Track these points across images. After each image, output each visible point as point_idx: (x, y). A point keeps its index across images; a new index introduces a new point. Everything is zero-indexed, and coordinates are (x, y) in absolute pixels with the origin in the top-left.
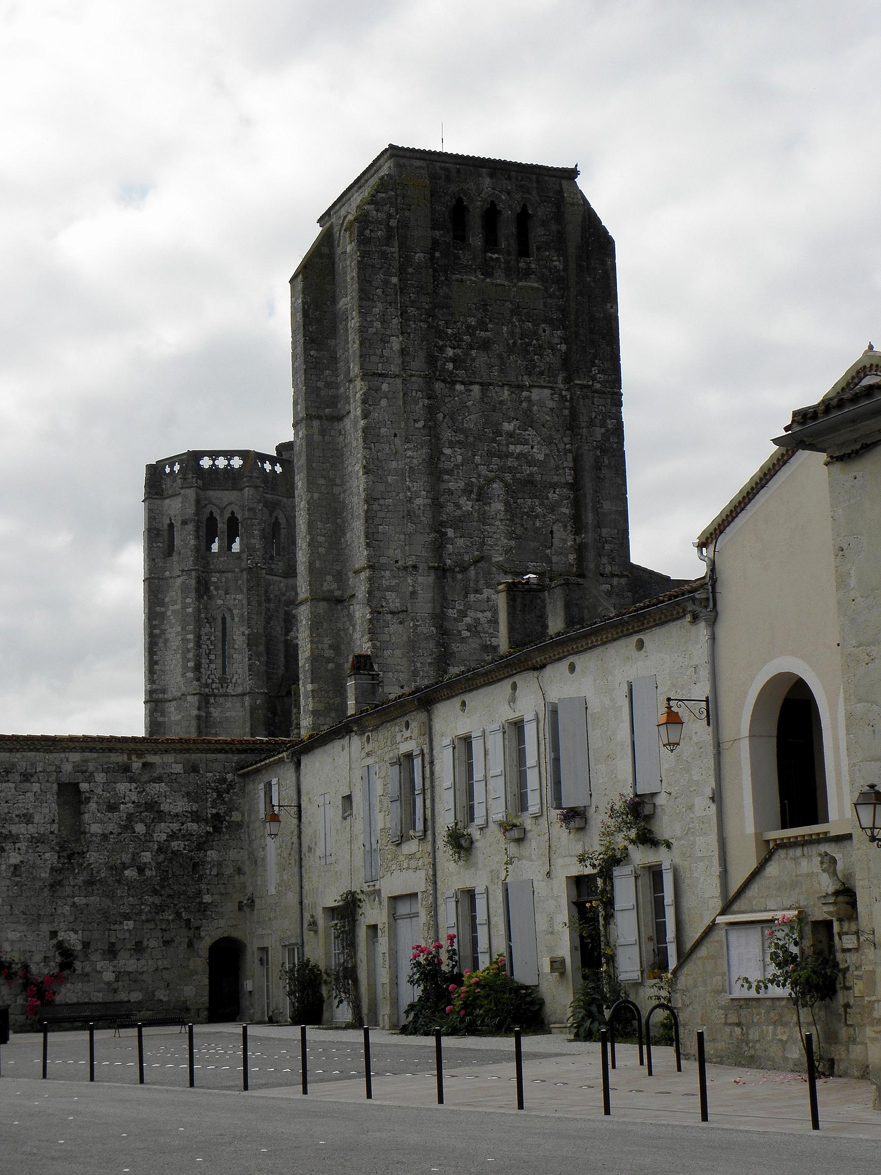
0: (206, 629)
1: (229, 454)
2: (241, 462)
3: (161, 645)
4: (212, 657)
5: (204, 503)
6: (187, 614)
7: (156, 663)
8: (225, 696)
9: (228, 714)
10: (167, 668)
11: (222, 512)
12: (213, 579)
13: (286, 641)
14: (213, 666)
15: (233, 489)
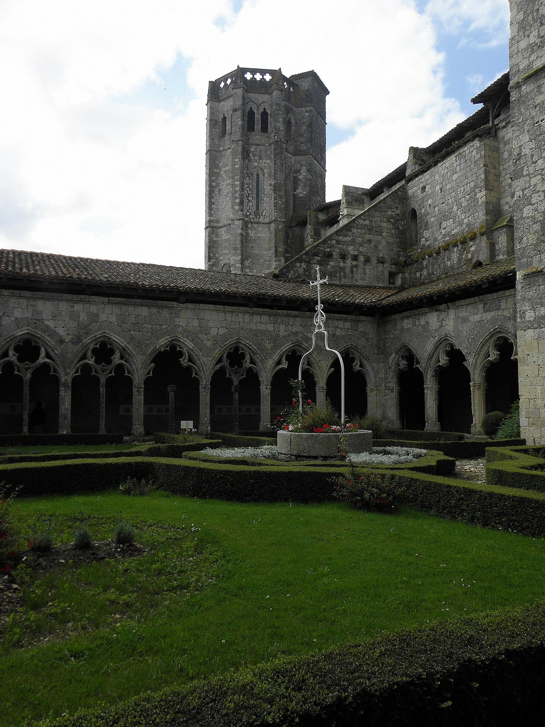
0: (247, 181)
1: (263, 72)
2: (271, 78)
3: (216, 192)
4: (250, 198)
5: (247, 101)
6: (236, 169)
7: (213, 204)
8: (258, 223)
9: (260, 235)
10: (220, 207)
11: (258, 107)
12: (252, 149)
13: (294, 195)
14: (250, 204)
15: (265, 93)
